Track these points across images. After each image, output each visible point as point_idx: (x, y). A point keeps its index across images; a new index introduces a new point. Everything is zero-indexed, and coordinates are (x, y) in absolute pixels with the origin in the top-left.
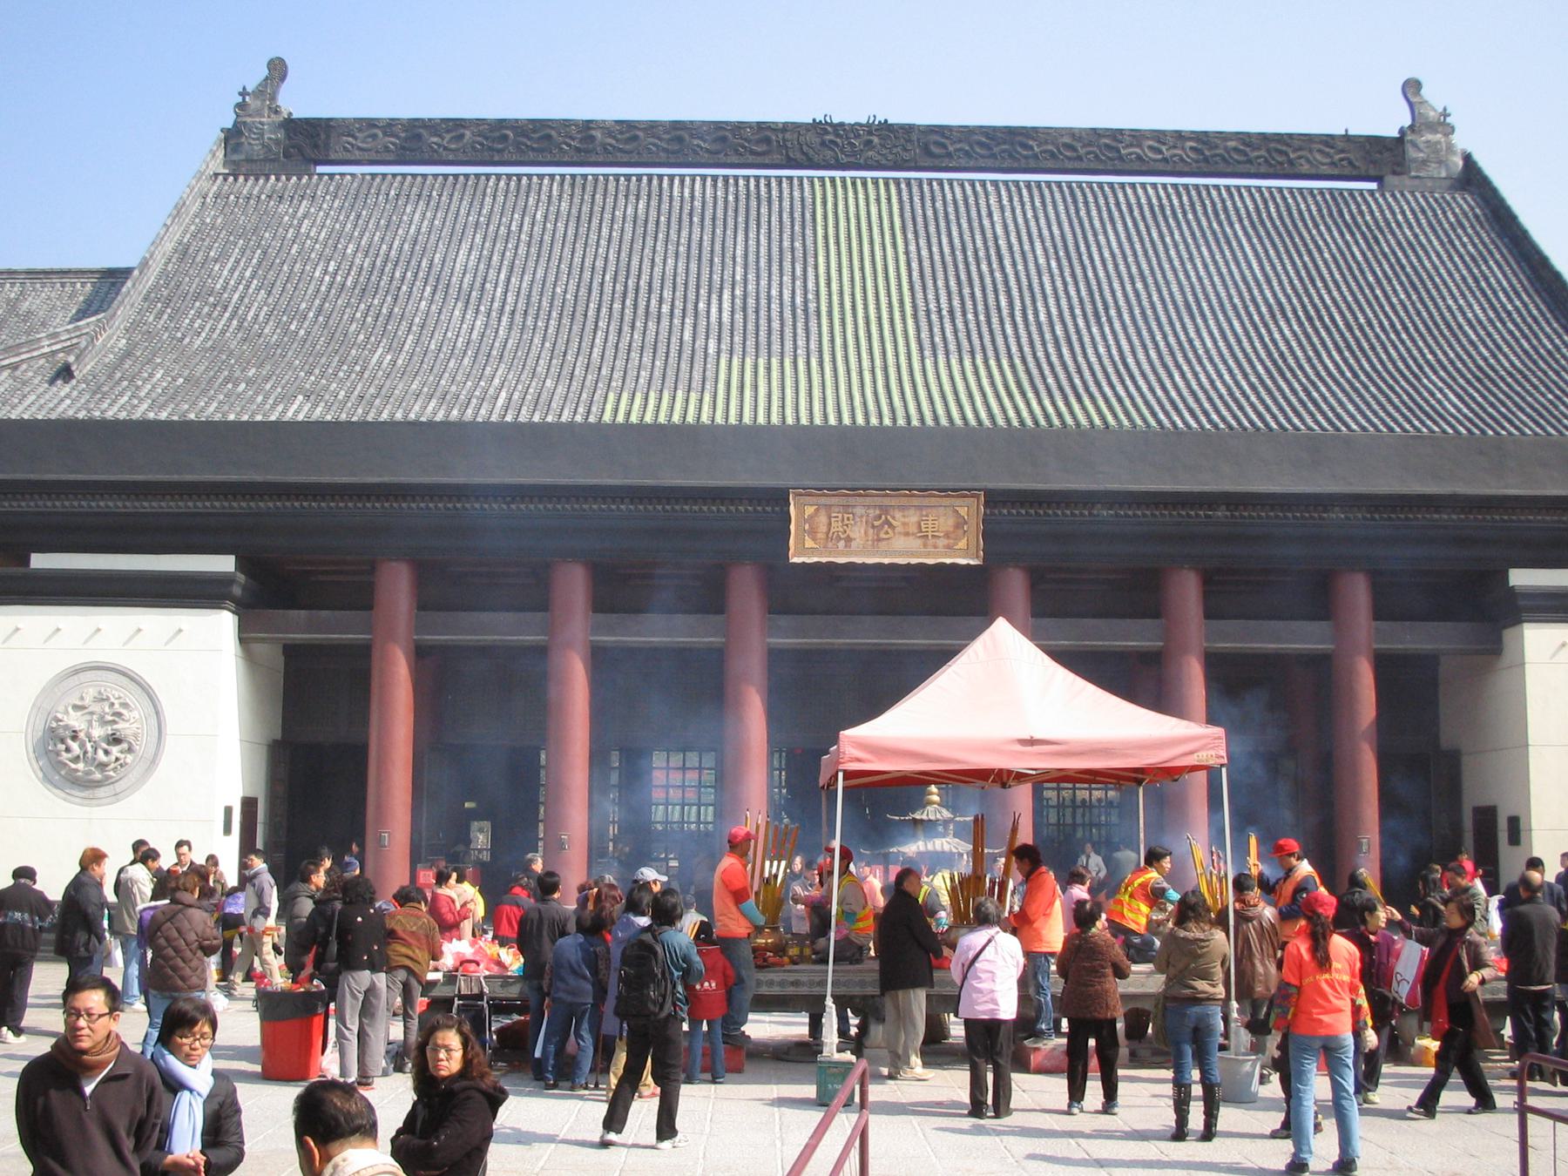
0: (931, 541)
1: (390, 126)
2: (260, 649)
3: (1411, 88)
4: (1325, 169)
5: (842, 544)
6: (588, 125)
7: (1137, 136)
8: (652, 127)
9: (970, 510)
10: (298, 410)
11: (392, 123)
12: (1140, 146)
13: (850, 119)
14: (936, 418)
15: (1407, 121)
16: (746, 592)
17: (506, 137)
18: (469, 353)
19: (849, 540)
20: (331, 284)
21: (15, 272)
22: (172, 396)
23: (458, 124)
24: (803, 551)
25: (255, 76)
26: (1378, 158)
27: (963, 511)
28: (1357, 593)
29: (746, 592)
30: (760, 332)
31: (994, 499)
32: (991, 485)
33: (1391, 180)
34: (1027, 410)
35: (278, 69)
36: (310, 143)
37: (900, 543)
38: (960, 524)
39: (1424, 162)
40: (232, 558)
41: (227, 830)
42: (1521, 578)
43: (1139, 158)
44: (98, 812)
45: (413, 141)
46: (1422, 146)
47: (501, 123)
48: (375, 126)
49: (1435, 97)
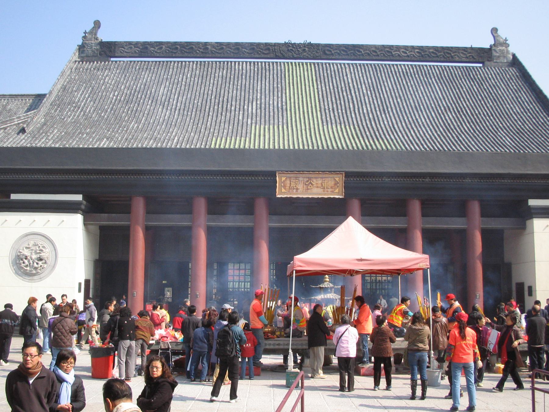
0: (326, 190)
1: (136, 44)
2: (91, 227)
3: (494, 31)
4: (464, 59)
5: (295, 191)
6: (206, 44)
7: (398, 48)
8: (228, 44)
9: (340, 179)
10: (104, 144)
11: (137, 43)
12: (399, 51)
13: (297, 42)
14: (328, 146)
15: (492, 42)
16: (261, 207)
17: (177, 48)
18: (164, 124)
19: (297, 189)
20: (116, 100)
21: (5, 95)
22: (60, 139)
23: (160, 44)
24: (281, 193)
25: (89, 27)
26: (482, 55)
27: (337, 179)
28: (475, 208)
29: (261, 207)
30: (266, 116)
31: (348, 175)
32: (347, 170)
33: (487, 63)
34: (360, 144)
35: (97, 24)
36: (109, 50)
37: (315, 190)
38: (336, 183)
39: (499, 57)
40: (81, 196)
41: (80, 291)
42: (532, 202)
43: (399, 55)
44: (34, 284)
45: (145, 49)
46: (498, 51)
47: (175, 43)
48: (131, 44)
49: (502, 34)
